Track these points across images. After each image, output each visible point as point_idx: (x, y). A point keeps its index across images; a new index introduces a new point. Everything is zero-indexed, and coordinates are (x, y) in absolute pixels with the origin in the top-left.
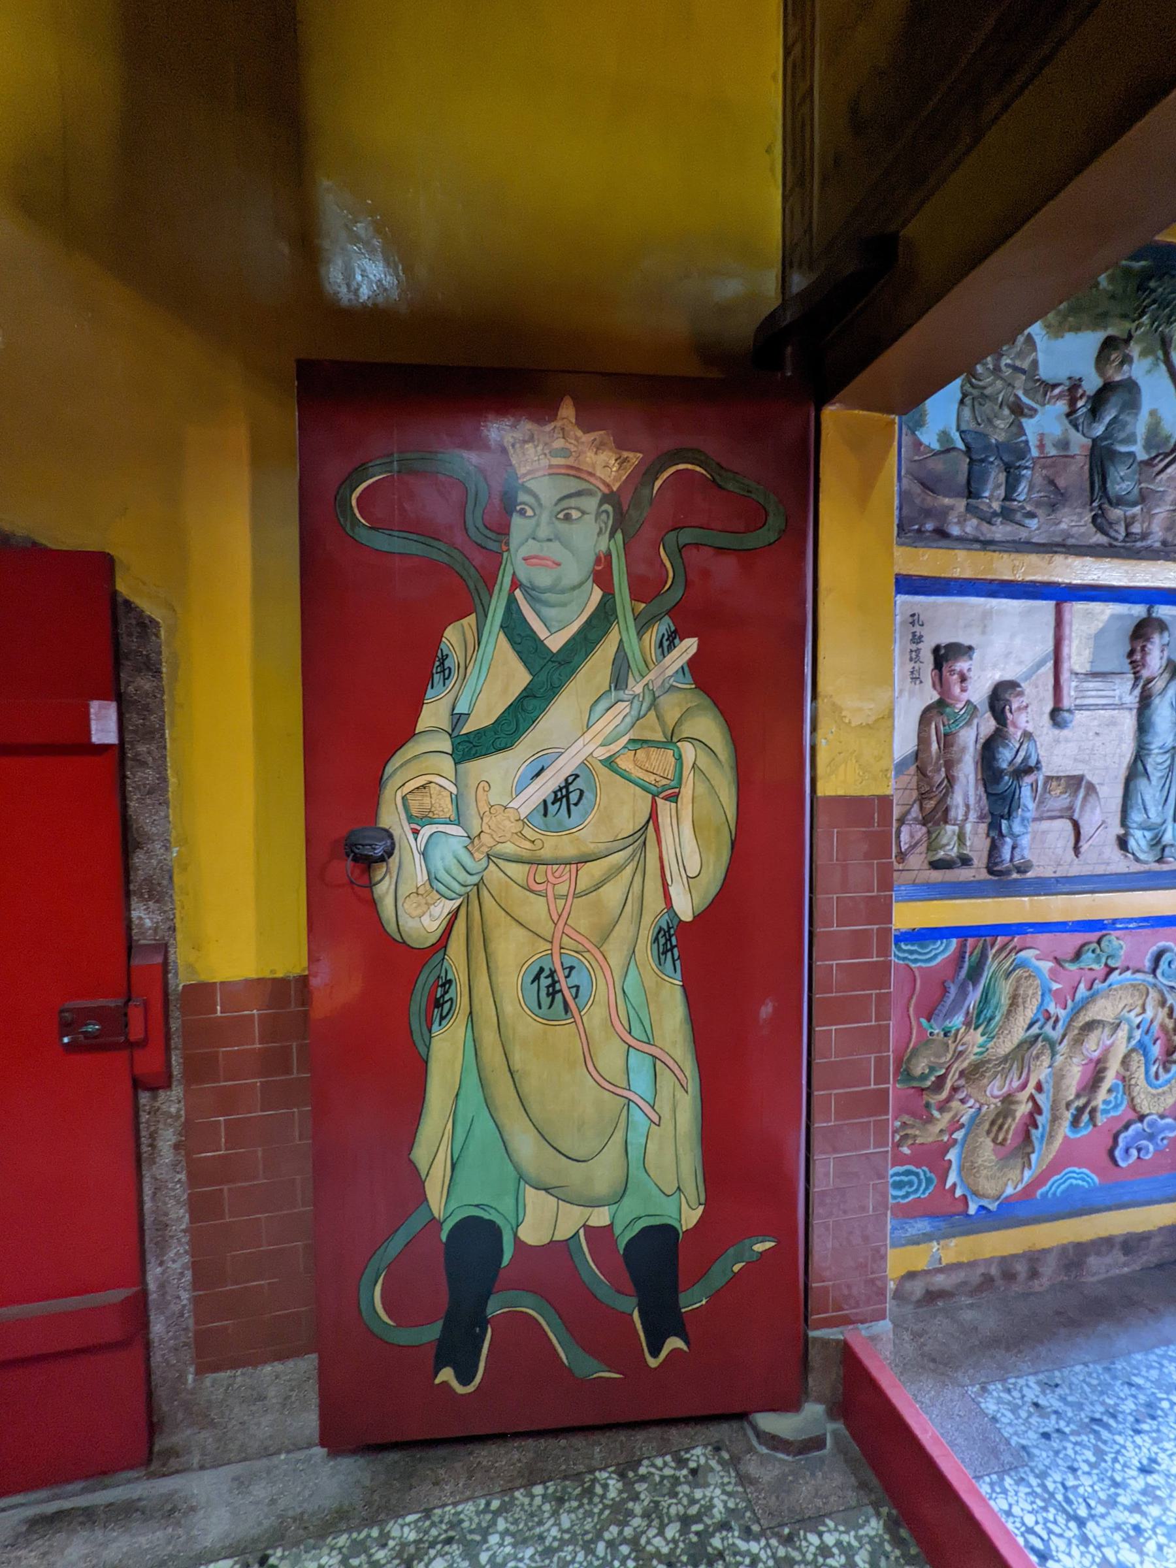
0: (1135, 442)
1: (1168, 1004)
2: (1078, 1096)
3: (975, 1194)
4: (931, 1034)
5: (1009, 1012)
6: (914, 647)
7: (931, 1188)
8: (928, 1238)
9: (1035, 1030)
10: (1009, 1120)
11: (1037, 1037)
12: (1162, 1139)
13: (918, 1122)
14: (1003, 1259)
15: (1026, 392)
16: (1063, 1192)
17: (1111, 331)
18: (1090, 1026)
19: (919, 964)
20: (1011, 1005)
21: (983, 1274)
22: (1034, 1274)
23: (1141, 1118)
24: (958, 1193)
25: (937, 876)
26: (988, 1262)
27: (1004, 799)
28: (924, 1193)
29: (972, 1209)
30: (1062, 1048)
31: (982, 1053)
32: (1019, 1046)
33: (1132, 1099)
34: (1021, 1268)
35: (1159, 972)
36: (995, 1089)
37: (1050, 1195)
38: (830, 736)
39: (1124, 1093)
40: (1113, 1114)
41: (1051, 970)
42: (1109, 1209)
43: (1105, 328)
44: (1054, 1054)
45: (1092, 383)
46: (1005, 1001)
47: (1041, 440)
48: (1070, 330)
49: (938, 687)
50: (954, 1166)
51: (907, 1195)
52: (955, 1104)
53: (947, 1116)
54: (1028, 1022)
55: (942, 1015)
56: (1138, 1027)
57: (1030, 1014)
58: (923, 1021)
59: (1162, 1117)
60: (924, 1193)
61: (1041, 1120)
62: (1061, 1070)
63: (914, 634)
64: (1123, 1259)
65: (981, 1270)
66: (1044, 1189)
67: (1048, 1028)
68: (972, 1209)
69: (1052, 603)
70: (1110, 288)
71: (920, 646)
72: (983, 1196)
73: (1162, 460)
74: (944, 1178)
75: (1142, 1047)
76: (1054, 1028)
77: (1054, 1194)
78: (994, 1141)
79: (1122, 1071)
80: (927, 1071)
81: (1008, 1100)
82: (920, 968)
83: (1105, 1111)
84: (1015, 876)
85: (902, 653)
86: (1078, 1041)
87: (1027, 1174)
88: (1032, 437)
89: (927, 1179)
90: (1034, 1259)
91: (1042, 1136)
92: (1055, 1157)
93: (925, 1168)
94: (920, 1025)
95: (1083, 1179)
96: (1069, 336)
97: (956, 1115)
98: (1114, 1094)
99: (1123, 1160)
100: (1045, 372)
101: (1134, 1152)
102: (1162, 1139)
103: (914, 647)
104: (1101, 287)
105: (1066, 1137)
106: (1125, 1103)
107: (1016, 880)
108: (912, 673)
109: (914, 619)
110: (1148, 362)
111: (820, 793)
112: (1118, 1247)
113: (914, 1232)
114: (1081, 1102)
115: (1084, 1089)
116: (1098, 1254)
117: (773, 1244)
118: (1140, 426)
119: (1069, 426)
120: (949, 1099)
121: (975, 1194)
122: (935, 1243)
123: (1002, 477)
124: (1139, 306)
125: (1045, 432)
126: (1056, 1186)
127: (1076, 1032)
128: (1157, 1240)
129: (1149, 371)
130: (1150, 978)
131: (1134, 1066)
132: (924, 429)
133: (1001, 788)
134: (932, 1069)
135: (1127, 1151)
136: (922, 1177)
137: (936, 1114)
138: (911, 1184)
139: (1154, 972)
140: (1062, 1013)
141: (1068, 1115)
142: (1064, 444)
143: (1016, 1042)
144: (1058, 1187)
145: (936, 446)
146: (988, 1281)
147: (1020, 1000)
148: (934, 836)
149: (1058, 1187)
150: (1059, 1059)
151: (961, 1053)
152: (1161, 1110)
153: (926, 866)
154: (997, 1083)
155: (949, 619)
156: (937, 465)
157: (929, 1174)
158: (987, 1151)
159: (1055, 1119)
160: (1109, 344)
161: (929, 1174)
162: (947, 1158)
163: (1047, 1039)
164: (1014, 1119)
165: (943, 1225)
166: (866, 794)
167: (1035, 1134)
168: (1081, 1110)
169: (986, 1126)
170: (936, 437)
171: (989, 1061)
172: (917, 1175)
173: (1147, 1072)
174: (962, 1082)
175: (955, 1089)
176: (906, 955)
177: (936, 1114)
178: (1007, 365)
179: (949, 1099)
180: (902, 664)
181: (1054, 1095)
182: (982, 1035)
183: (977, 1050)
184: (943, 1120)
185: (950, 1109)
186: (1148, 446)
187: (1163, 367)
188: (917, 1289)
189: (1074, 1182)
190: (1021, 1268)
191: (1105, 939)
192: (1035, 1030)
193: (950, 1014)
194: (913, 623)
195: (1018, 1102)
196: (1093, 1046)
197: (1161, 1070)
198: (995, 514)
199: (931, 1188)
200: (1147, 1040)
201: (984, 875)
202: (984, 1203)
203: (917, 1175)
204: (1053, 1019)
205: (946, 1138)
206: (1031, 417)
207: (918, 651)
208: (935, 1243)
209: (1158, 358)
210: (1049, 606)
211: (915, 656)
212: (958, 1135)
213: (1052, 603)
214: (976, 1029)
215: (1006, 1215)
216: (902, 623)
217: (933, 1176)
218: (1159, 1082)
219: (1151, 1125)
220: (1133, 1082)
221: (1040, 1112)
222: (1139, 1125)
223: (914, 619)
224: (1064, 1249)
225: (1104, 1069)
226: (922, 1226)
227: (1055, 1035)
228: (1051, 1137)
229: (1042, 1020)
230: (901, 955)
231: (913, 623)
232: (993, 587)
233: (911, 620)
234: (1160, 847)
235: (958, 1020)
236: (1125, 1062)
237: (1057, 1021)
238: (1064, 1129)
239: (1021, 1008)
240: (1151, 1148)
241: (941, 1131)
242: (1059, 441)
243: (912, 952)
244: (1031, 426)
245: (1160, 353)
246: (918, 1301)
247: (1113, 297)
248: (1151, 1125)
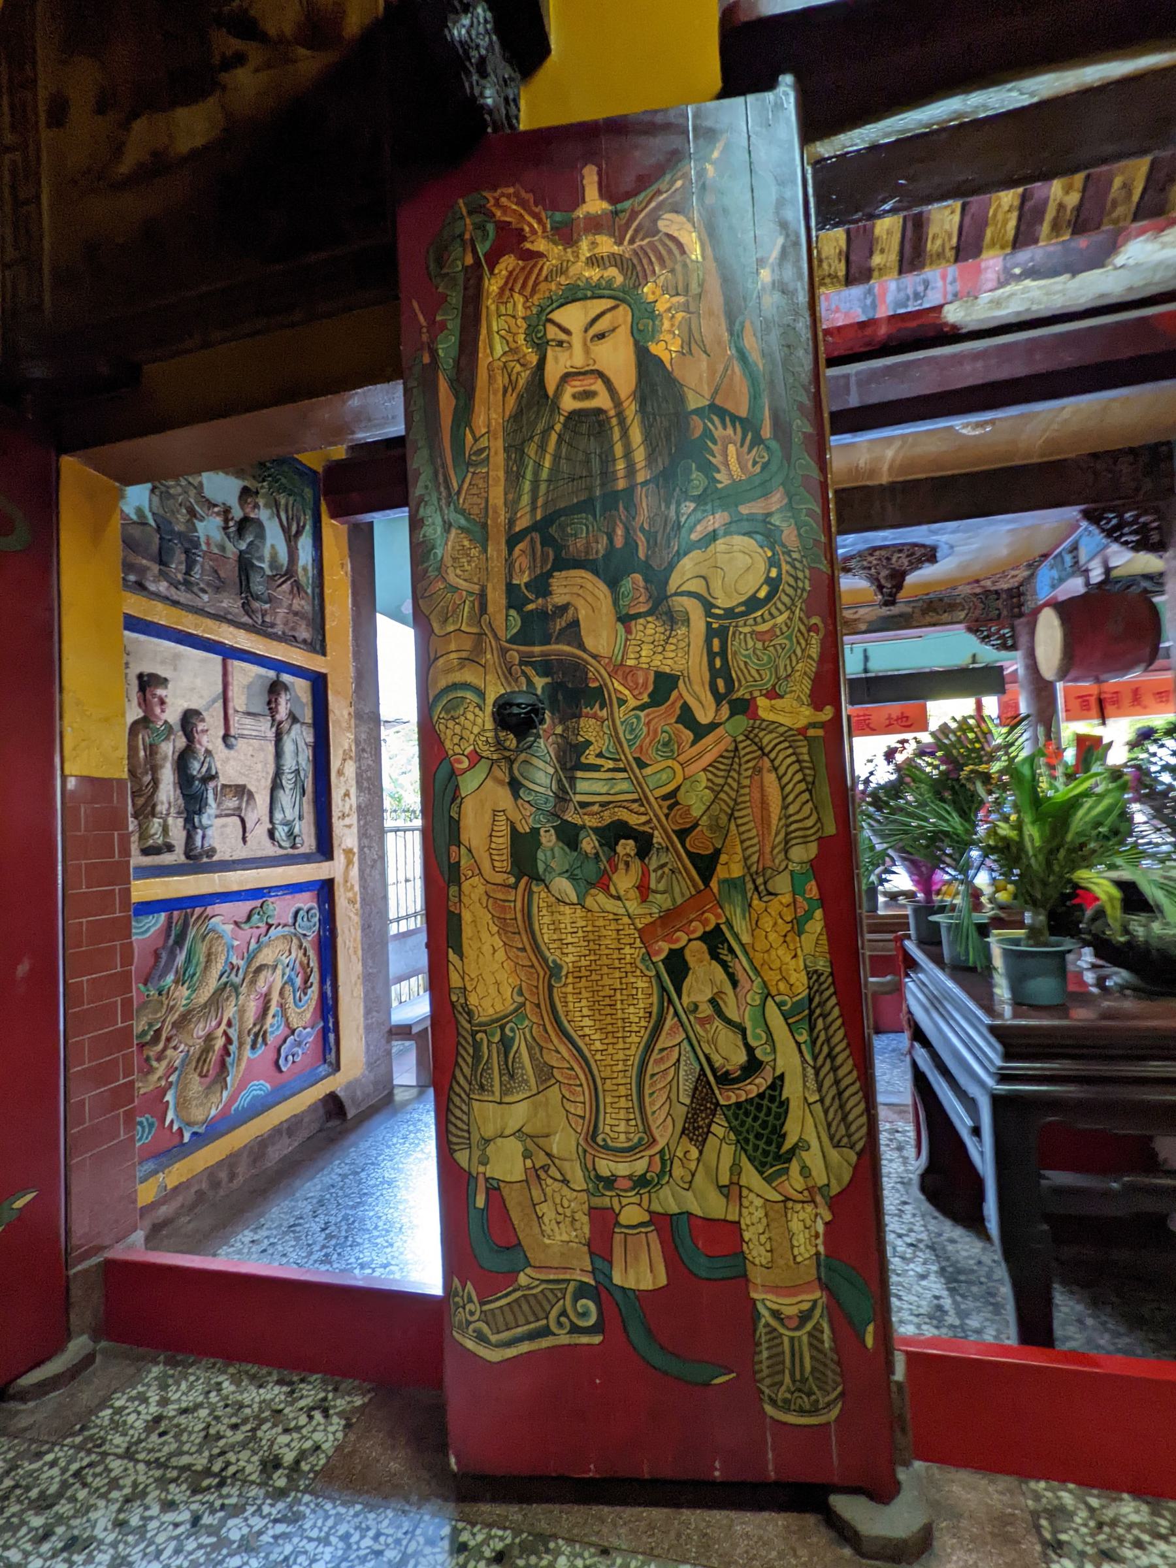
8: (155, 1173)
9: (224, 979)
18: (259, 969)
30: (243, 989)
36: (200, 1030)
50: (171, 1106)
53: (164, 1063)
57: (220, 967)
158: (196, 1085)
163: (232, 985)
169: (194, 1064)
190: (223, 1175)
192: (224, 979)
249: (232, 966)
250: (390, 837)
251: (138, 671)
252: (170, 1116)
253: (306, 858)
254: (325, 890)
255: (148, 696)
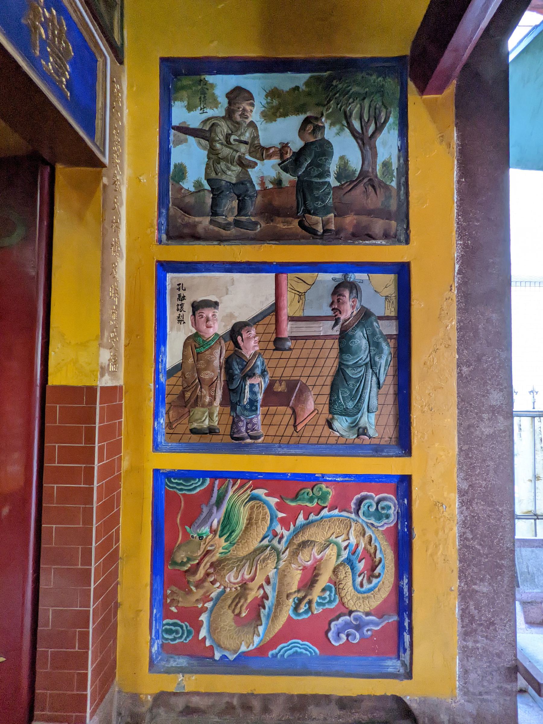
0: (329, 176)
1: (367, 535)
2: (299, 591)
3: (219, 646)
4: (192, 536)
5: (246, 528)
6: (180, 303)
7: (191, 638)
8: (182, 670)
9: (266, 542)
10: (242, 601)
11: (267, 547)
12: (367, 631)
13: (181, 593)
14: (242, 696)
15: (250, 154)
16: (289, 656)
17: (308, 114)
18: (304, 544)
19: (184, 492)
20: (248, 524)
21: (228, 702)
22: (266, 709)
23: (350, 613)
24: (208, 644)
25: (195, 438)
26: (232, 695)
27: (236, 393)
28: (186, 639)
29: (217, 656)
30: (285, 556)
31: (226, 553)
32: (255, 551)
33: (341, 598)
34: (256, 704)
35: (361, 513)
36: (232, 578)
37: (279, 656)
38: (57, 350)
39: (336, 594)
40: (327, 606)
41: (277, 504)
42: (318, 674)
43: (305, 113)
44: (279, 559)
45: (297, 144)
46: (243, 522)
47: (262, 181)
48: (280, 116)
49: (194, 325)
50: (205, 625)
51: (174, 639)
52: (207, 584)
53: (201, 592)
54: (261, 536)
55: (196, 525)
56: (345, 548)
57: (262, 533)
58: (187, 527)
59: (367, 614)
60: (186, 639)
61: (267, 603)
62: (284, 571)
63: (179, 295)
64: (338, 712)
65: (227, 699)
66: (274, 651)
67: (275, 542)
68: (217, 656)
69: (273, 275)
70: (307, 90)
71: (183, 302)
72: (225, 649)
73: (349, 185)
74: (198, 632)
75: (349, 561)
76: (279, 542)
77: (283, 656)
78: (233, 612)
79: (334, 578)
80: (185, 560)
81: (244, 586)
82: (184, 495)
83: (319, 604)
84: (249, 441)
85: (172, 306)
86: (295, 554)
87: (257, 640)
88: (256, 181)
89: (188, 631)
90: (267, 701)
91: (269, 615)
92: (280, 631)
93: (186, 623)
94: (185, 531)
95: (306, 650)
96: (280, 120)
97: (207, 592)
98: (328, 593)
99: (335, 641)
100: (263, 141)
101: (343, 636)
102: (367, 631)
103: (180, 302)
104: (301, 90)
105: (289, 617)
106: (337, 600)
107: (250, 444)
108: (179, 317)
109: (180, 287)
110: (335, 129)
111: (53, 381)
112: (334, 703)
113: (174, 664)
114: (301, 595)
115: (305, 586)
116: (318, 705)
117: (4, 659)
118: (333, 167)
119: (281, 171)
120: (203, 580)
121: (219, 646)
122: (181, 675)
123: (235, 203)
124: (327, 97)
125: (265, 175)
126: (284, 650)
127: (295, 547)
128: (366, 704)
129: (338, 134)
130: (353, 516)
131: (341, 576)
132: (185, 181)
133: (234, 386)
134: (189, 560)
135: (338, 634)
136: (185, 628)
137: (193, 589)
138: (177, 632)
139: (357, 514)
140: (286, 533)
141: (291, 602)
142: (278, 182)
143: (252, 548)
144: (286, 651)
145: (192, 189)
146: (229, 708)
147: (253, 521)
148: (191, 414)
149: (286, 651)
150: (282, 564)
151: (208, 552)
152: (367, 609)
153: (188, 431)
154: (232, 574)
155: (200, 286)
156: (190, 200)
157: (189, 628)
158: (228, 619)
159: (279, 604)
160: (307, 121)
161: (189, 628)
162: (200, 619)
163: (274, 548)
164: (246, 600)
165: (195, 663)
166: (80, 385)
167: (264, 613)
168: (300, 600)
169: (229, 602)
170: (193, 184)
171: (229, 559)
172: (182, 627)
173: (354, 581)
174: (212, 570)
175: (208, 575)
176: (175, 486)
177: (193, 589)
178: (235, 140)
179: (203, 580)
180: (172, 313)
181: (279, 588)
182: (226, 541)
183: (221, 550)
184: (198, 594)
185: (203, 587)
186: (338, 178)
187: (347, 130)
188: (180, 703)
189: (299, 650)
190: (256, 704)
191: (316, 487)
192: (266, 542)
193: (199, 526)
194: (179, 289)
195: (251, 590)
196: (307, 558)
197: (365, 582)
198: (229, 224)
199: (191, 638)
200: (353, 558)
201: (228, 439)
202: (227, 654)
203: (182, 627)
204: (279, 536)
205: (200, 606)
206: (254, 167)
207: (182, 305)
208: (181, 675)
209: (344, 125)
210: (271, 276)
211: (180, 308)
212: (209, 605)
213: (273, 275)
214: (220, 536)
215: (241, 665)
216: (172, 289)
217: (192, 629)
218: (363, 589)
219: (356, 619)
220: (341, 586)
221: (267, 599)
222: (348, 617)
223: (180, 287)
224: (290, 697)
225: (317, 575)
226: (182, 661)
227: (281, 547)
228: (276, 617)
229: (271, 536)
230: (171, 485)
231: (179, 289)
232: (227, 266)
233: (178, 287)
234: (357, 428)
235: (205, 530)
236: (335, 571)
237: (282, 537)
238: (287, 611)
239: (255, 526)
240: (358, 636)
241: (197, 600)
242: (275, 180)
243: (177, 483)
244: (254, 174)
245: (345, 123)
246: (181, 712)
247: (309, 94)
248: (356, 619)
249: (275, 535)
250: (516, 420)
251: (192, 300)
252: (203, 633)
253: (377, 451)
254: (403, 484)
255: (197, 315)
